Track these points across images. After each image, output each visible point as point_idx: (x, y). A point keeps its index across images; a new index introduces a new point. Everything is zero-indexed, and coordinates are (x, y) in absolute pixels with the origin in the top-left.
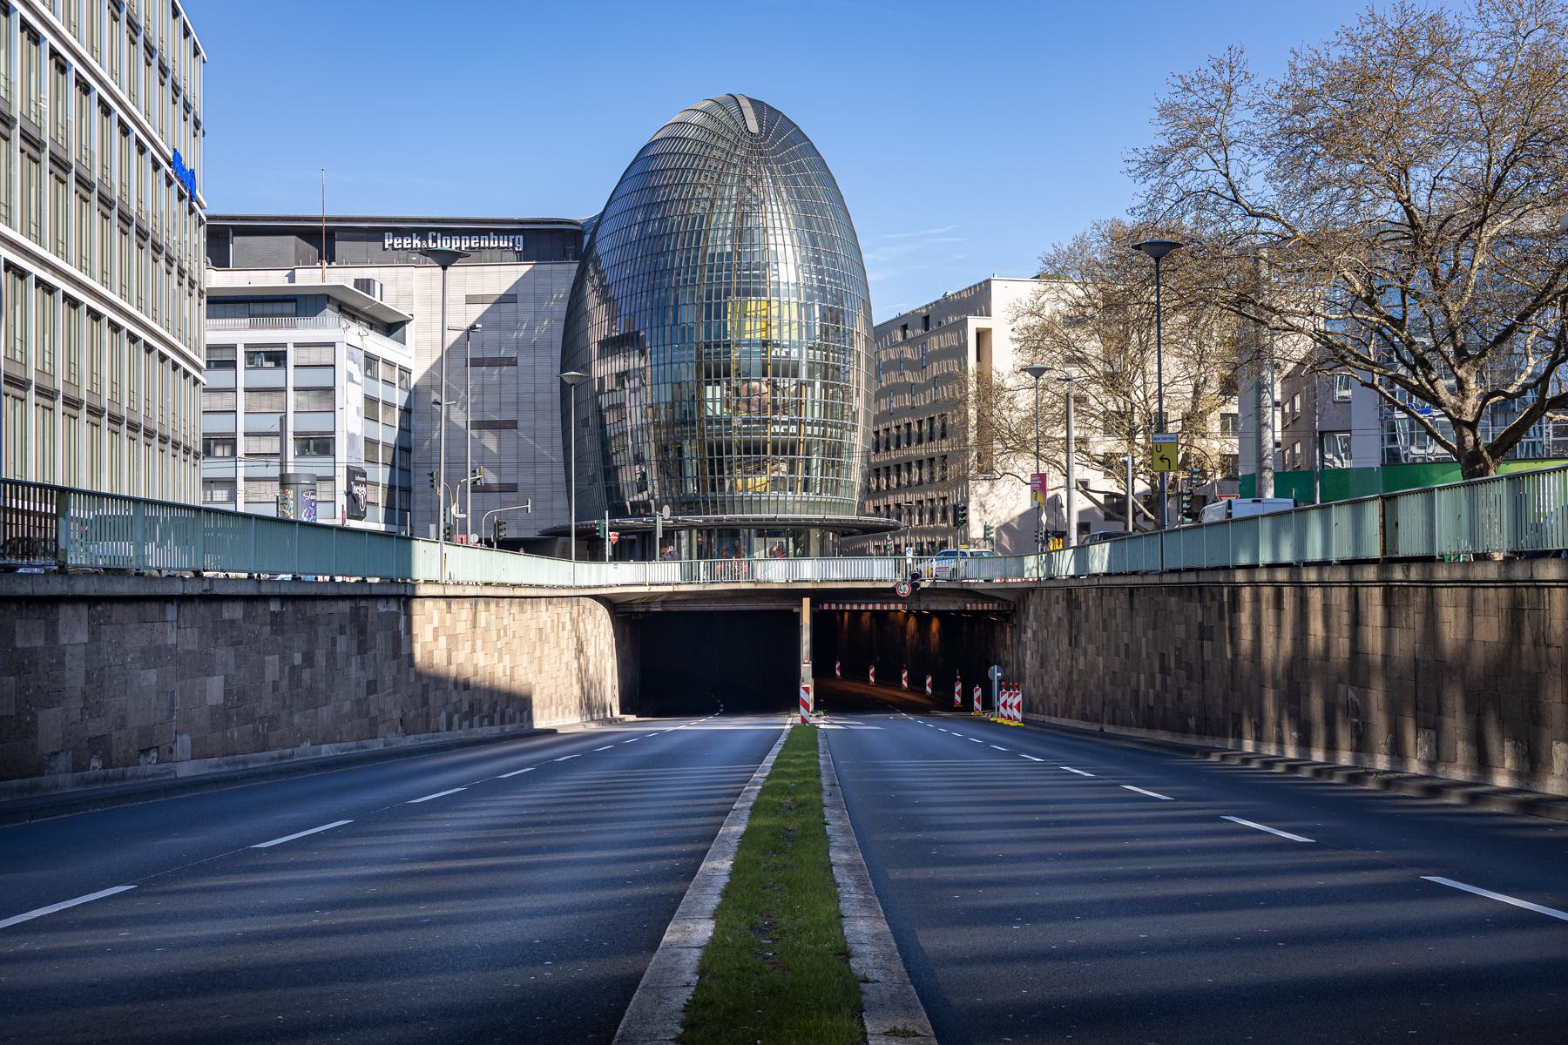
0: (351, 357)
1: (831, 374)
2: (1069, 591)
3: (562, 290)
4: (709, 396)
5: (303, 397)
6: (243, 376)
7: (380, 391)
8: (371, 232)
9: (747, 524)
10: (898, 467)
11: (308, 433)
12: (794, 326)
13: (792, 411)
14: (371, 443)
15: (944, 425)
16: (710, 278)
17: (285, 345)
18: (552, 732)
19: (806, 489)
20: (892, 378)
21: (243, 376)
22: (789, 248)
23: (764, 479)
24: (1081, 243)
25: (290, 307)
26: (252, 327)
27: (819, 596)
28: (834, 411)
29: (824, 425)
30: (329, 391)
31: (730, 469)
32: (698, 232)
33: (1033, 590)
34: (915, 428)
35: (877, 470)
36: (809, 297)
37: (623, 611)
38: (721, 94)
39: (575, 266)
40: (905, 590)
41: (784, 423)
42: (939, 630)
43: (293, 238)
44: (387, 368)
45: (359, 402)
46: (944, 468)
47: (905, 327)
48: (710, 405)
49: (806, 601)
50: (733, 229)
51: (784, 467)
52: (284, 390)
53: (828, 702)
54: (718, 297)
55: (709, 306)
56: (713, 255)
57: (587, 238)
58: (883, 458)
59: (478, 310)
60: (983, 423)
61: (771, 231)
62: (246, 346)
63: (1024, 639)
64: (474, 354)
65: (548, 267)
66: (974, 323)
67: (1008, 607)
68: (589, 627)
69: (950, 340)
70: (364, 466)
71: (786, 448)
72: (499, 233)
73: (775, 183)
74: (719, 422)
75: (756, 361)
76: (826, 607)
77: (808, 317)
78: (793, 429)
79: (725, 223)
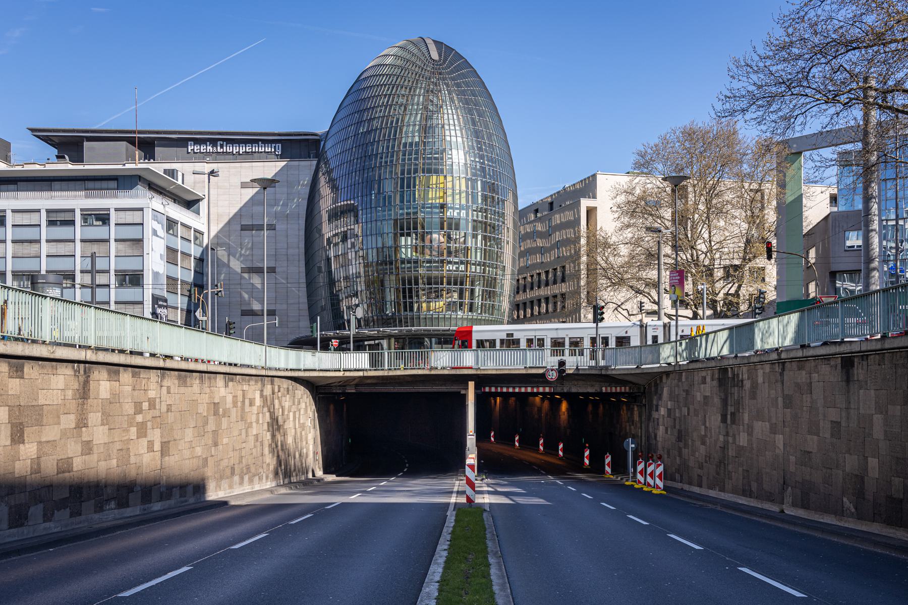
0: (155, 218)
1: (489, 229)
2: (724, 371)
3: (307, 180)
4: (403, 243)
5: (121, 246)
6: (79, 231)
7: (179, 245)
8: (179, 142)
9: (430, 335)
10: (532, 302)
11: (125, 271)
12: (464, 195)
13: (461, 255)
14: (172, 281)
15: (563, 273)
16: (404, 160)
17: (109, 209)
18: (222, 505)
19: (471, 310)
20: (529, 244)
21: (79, 231)
22: (460, 139)
23: (442, 303)
24: (665, 141)
25: (113, 184)
26: (87, 197)
27: (482, 380)
28: (491, 256)
29: (484, 264)
30: (139, 242)
31: (418, 296)
32: (396, 128)
33: (667, 374)
34: (543, 277)
35: (518, 305)
36: (474, 175)
37: (324, 392)
38: (414, 38)
39: (315, 163)
40: (552, 376)
41: (456, 263)
42: (568, 410)
43: (125, 143)
44: (184, 229)
45: (162, 250)
46: (563, 302)
47: (537, 211)
48: (403, 250)
49: (471, 385)
50: (420, 125)
51: (456, 295)
52: (108, 241)
53: (490, 465)
54: (409, 172)
55: (402, 180)
56: (405, 144)
57: (322, 143)
58: (521, 297)
59: (250, 193)
60: (592, 271)
61: (447, 127)
62: (82, 210)
63: (655, 415)
64: (244, 224)
65: (296, 163)
66: (585, 203)
67: (641, 389)
68: (287, 405)
69: (569, 216)
70: (165, 294)
71: (458, 281)
72: (265, 142)
73: (450, 94)
74: (409, 262)
75: (436, 219)
76: (487, 389)
77: (473, 188)
78: (462, 267)
79: (415, 121)
